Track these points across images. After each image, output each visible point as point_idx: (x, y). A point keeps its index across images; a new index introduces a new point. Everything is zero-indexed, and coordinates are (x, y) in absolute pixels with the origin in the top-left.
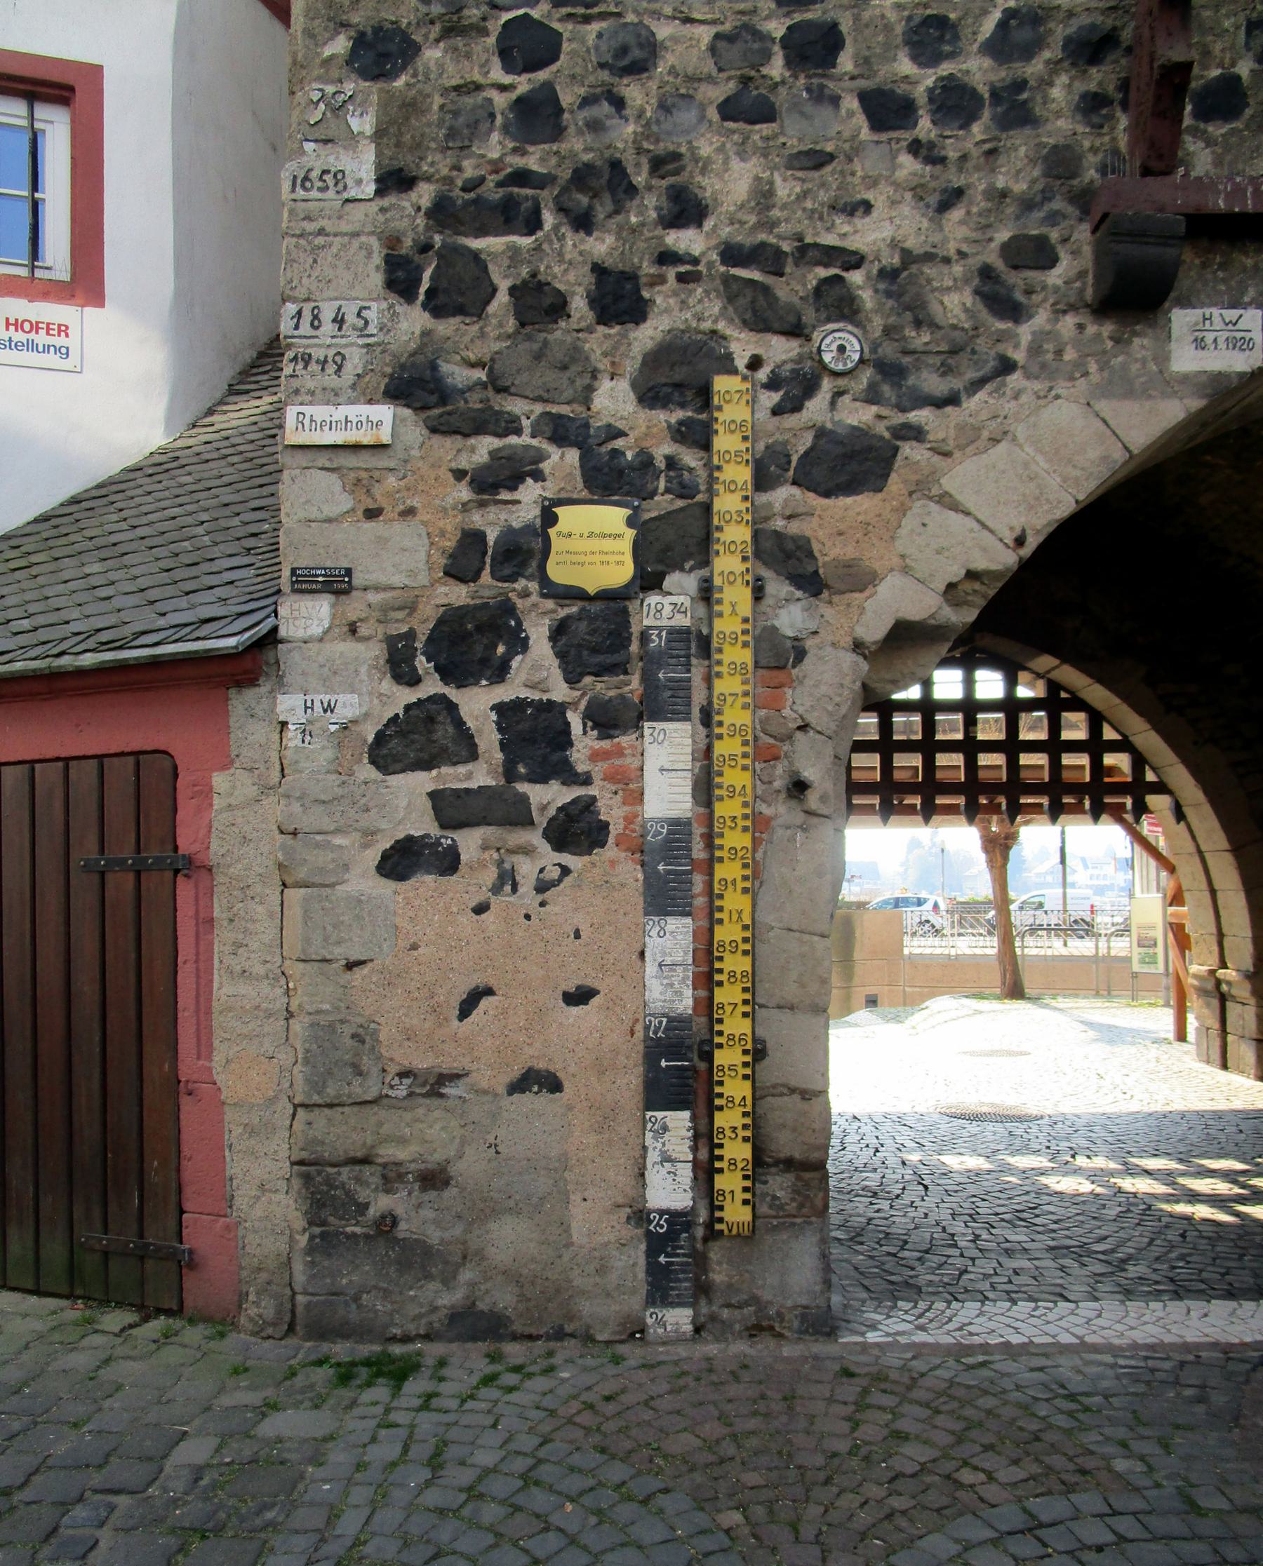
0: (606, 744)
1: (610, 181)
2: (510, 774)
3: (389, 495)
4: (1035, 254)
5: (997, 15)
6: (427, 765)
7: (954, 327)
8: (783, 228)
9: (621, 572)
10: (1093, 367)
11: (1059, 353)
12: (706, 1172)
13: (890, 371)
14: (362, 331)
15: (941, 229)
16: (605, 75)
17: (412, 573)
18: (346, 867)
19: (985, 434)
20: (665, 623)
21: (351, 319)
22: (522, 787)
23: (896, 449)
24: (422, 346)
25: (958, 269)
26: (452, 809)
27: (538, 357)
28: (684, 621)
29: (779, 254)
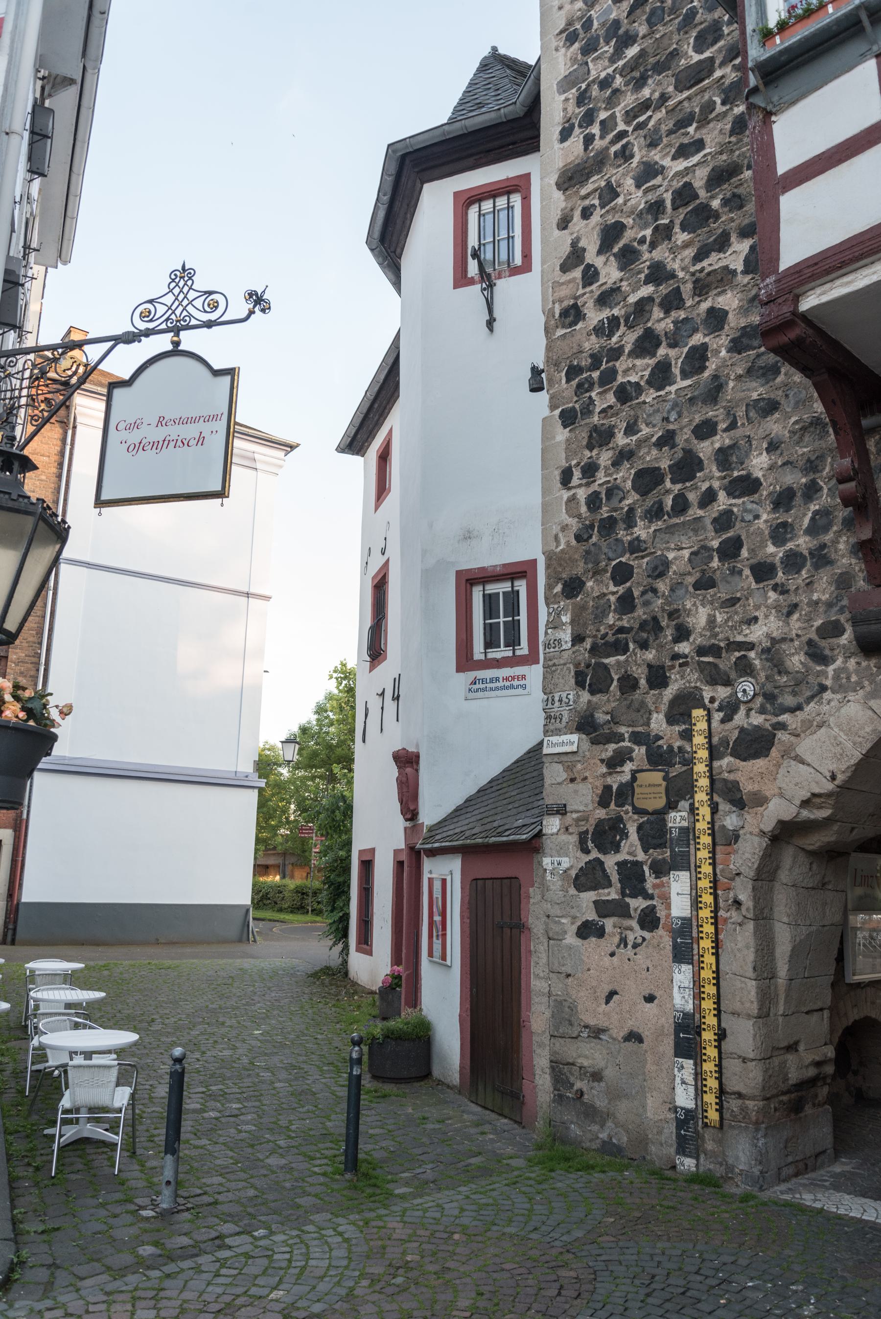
0: (658, 881)
1: (653, 626)
2: (623, 894)
3: (578, 772)
4: (832, 630)
5: (810, 515)
6: (594, 888)
7: (797, 672)
8: (721, 636)
9: (660, 803)
10: (866, 683)
11: (848, 678)
12: (700, 1091)
13: (770, 697)
14: (568, 704)
15: (788, 624)
16: (650, 580)
17: (586, 805)
18: (565, 932)
19: (815, 723)
20: (677, 825)
21: (564, 699)
22: (627, 900)
23: (775, 735)
24: (588, 707)
25: (797, 643)
26: (603, 908)
27: (629, 707)
28: (685, 824)
29: (720, 648)
